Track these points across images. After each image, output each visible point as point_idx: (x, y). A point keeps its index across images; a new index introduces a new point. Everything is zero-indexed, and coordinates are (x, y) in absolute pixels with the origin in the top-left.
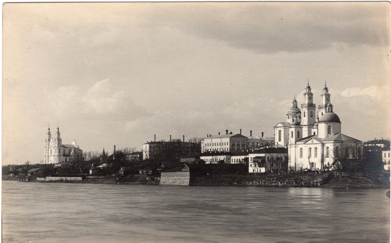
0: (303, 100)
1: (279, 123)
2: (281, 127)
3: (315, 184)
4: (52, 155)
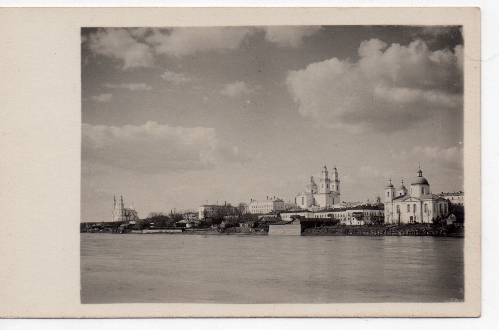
0: (319, 177)
1: (302, 192)
2: (304, 195)
3: (440, 233)
4: (117, 215)
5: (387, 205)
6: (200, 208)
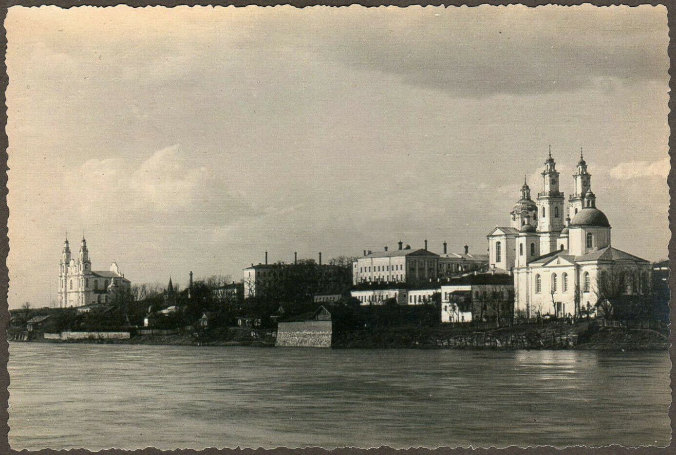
1: (496, 229)
2: (500, 235)
5: (518, 273)
6: (246, 273)
